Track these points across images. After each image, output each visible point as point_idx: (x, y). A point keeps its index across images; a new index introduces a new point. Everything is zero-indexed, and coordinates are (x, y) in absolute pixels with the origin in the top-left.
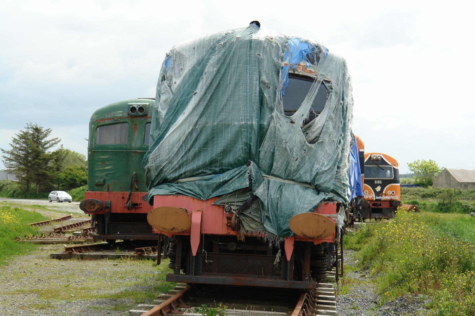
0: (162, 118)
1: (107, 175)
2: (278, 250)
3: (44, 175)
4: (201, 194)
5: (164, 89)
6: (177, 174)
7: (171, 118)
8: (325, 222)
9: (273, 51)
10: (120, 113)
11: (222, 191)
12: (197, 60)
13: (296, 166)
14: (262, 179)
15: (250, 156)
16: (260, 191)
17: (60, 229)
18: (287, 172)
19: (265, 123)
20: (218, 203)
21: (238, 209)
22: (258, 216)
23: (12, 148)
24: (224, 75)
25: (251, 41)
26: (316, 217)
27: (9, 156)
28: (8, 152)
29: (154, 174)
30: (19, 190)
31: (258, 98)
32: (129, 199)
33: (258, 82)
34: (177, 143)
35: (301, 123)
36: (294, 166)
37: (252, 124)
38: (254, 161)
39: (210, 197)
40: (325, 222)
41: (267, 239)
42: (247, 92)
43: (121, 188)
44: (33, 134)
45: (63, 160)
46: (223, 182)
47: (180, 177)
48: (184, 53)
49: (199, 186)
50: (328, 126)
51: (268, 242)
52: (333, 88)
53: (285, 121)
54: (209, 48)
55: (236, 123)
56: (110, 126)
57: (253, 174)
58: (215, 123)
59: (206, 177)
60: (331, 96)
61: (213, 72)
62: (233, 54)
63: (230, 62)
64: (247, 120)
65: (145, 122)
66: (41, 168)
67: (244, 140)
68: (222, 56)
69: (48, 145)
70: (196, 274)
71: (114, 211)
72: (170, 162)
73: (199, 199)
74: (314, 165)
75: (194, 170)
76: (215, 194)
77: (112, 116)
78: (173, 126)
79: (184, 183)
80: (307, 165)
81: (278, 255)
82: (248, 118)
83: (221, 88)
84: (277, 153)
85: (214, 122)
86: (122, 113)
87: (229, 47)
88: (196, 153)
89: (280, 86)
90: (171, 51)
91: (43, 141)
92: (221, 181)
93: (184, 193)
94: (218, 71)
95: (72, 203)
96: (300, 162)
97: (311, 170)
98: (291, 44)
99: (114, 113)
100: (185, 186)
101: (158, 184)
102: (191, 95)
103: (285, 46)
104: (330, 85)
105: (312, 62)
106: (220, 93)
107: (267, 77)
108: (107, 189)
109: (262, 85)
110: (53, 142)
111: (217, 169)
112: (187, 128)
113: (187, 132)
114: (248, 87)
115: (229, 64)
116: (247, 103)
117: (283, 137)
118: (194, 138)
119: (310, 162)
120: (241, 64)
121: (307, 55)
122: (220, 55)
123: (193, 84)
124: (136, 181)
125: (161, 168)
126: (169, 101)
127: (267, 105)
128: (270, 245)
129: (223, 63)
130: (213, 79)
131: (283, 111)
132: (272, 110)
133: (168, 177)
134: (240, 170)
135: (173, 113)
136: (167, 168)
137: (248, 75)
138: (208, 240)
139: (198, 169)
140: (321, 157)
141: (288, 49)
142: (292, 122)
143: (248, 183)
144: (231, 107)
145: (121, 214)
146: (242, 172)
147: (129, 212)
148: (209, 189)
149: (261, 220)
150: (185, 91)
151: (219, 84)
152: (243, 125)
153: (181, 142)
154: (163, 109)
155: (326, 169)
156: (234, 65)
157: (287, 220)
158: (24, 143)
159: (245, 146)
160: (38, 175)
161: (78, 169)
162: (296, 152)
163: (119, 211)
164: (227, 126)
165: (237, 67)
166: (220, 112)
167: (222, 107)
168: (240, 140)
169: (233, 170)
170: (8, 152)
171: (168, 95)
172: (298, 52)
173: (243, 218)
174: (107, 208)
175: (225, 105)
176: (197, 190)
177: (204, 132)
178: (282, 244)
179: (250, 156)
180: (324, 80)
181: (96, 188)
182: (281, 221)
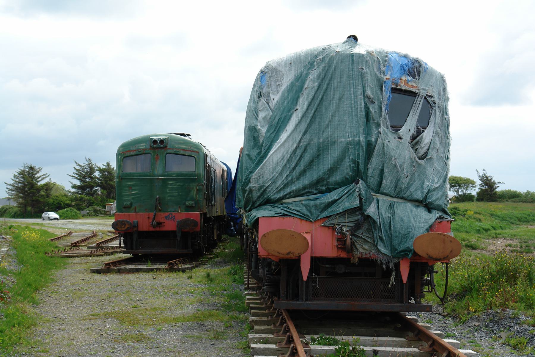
0: (262, 136)
1: (133, 199)
2: (393, 271)
3: (37, 201)
4: (309, 215)
5: (262, 106)
6: (281, 194)
7: (273, 135)
8: (451, 242)
9: (375, 65)
10: (143, 146)
11: (332, 211)
12: (295, 76)
13: (406, 184)
14: (372, 198)
15: (358, 174)
16: (371, 210)
17: (75, 243)
18: (397, 189)
19: (373, 139)
20: (327, 224)
21: (350, 230)
22: (370, 236)
23: (13, 182)
24: (326, 89)
25: (352, 55)
26: (442, 236)
27: (10, 187)
28: (10, 185)
29: (256, 195)
30: (19, 212)
31: (364, 113)
32: (154, 219)
33: (362, 97)
34: (280, 162)
35: (409, 139)
36: (404, 184)
37: (360, 141)
38: (362, 179)
39: (319, 218)
40: (451, 242)
41: (381, 261)
42: (351, 108)
43: (146, 209)
44: (28, 172)
45: (51, 189)
46: (332, 201)
47: (285, 197)
48: (281, 69)
49: (306, 206)
50: (435, 142)
51: (382, 263)
52: (436, 102)
53: (393, 137)
54: (307, 63)
55: (343, 140)
56: (138, 156)
57: (363, 192)
58: (321, 140)
59: (311, 197)
60: (435, 110)
61: (314, 87)
62: (335, 68)
63: (332, 77)
64: (354, 136)
65: (165, 153)
66: (35, 196)
67: (351, 157)
68: (323, 70)
69: (40, 179)
70: (307, 300)
71: (141, 229)
72: (274, 182)
73: (308, 220)
74: (424, 182)
75: (299, 190)
76: (324, 215)
77: (137, 148)
78: (276, 144)
79: (289, 203)
80: (417, 182)
81: (393, 278)
82: (355, 134)
83: (324, 104)
84: (386, 170)
85: (319, 138)
86: (145, 146)
87: (329, 61)
88: (301, 171)
89: (385, 101)
90: (265, 67)
91: (36, 176)
92: (330, 200)
93: (291, 214)
94: (319, 86)
95: (60, 221)
96: (410, 179)
97: (422, 188)
98: (391, 58)
99: (138, 145)
100: (290, 206)
101: (260, 205)
102: (291, 112)
103: (386, 61)
104: (433, 99)
105: (414, 77)
106: (324, 108)
107: (371, 91)
108: (134, 211)
109: (367, 100)
110: (44, 177)
111: (324, 188)
112: (290, 145)
113: (291, 150)
114: (353, 102)
115: (331, 79)
116: (352, 118)
117: (393, 153)
118: (299, 157)
119: (420, 179)
120: (344, 79)
121: (409, 69)
122: (320, 70)
123: (293, 100)
124: (159, 203)
125: (265, 188)
126: (268, 118)
127: (374, 120)
128: (384, 266)
129: (324, 78)
130: (315, 94)
131: (390, 127)
132: (378, 125)
133: (272, 198)
134: (349, 189)
135: (275, 130)
136: (271, 188)
137: (352, 90)
138: (317, 262)
139: (304, 188)
140: (430, 173)
141: (389, 63)
142: (400, 138)
143: (358, 202)
144: (337, 123)
145: (146, 232)
146: (351, 191)
147: (154, 230)
148: (318, 210)
149: (374, 241)
150: (285, 107)
151: (322, 99)
152: (350, 141)
153: (286, 161)
154: (262, 127)
155: (437, 186)
156: (336, 80)
157: (403, 240)
158: (22, 178)
159: (353, 163)
160: (33, 201)
161: (62, 196)
162: (407, 169)
163: (145, 229)
164: (333, 143)
165: (340, 82)
166: (325, 129)
167: (327, 123)
168: (347, 157)
169: (341, 189)
170: (10, 185)
171: (267, 112)
172: (399, 66)
173: (355, 239)
174: (135, 227)
175: (330, 121)
176: (305, 211)
177: (309, 150)
178: (397, 266)
179: (358, 174)
180: (427, 95)
181: (124, 210)
182: (396, 241)
